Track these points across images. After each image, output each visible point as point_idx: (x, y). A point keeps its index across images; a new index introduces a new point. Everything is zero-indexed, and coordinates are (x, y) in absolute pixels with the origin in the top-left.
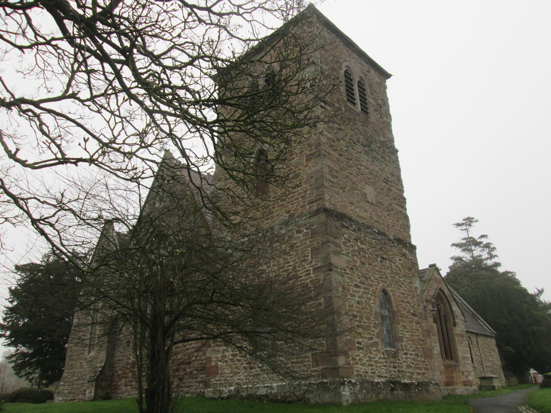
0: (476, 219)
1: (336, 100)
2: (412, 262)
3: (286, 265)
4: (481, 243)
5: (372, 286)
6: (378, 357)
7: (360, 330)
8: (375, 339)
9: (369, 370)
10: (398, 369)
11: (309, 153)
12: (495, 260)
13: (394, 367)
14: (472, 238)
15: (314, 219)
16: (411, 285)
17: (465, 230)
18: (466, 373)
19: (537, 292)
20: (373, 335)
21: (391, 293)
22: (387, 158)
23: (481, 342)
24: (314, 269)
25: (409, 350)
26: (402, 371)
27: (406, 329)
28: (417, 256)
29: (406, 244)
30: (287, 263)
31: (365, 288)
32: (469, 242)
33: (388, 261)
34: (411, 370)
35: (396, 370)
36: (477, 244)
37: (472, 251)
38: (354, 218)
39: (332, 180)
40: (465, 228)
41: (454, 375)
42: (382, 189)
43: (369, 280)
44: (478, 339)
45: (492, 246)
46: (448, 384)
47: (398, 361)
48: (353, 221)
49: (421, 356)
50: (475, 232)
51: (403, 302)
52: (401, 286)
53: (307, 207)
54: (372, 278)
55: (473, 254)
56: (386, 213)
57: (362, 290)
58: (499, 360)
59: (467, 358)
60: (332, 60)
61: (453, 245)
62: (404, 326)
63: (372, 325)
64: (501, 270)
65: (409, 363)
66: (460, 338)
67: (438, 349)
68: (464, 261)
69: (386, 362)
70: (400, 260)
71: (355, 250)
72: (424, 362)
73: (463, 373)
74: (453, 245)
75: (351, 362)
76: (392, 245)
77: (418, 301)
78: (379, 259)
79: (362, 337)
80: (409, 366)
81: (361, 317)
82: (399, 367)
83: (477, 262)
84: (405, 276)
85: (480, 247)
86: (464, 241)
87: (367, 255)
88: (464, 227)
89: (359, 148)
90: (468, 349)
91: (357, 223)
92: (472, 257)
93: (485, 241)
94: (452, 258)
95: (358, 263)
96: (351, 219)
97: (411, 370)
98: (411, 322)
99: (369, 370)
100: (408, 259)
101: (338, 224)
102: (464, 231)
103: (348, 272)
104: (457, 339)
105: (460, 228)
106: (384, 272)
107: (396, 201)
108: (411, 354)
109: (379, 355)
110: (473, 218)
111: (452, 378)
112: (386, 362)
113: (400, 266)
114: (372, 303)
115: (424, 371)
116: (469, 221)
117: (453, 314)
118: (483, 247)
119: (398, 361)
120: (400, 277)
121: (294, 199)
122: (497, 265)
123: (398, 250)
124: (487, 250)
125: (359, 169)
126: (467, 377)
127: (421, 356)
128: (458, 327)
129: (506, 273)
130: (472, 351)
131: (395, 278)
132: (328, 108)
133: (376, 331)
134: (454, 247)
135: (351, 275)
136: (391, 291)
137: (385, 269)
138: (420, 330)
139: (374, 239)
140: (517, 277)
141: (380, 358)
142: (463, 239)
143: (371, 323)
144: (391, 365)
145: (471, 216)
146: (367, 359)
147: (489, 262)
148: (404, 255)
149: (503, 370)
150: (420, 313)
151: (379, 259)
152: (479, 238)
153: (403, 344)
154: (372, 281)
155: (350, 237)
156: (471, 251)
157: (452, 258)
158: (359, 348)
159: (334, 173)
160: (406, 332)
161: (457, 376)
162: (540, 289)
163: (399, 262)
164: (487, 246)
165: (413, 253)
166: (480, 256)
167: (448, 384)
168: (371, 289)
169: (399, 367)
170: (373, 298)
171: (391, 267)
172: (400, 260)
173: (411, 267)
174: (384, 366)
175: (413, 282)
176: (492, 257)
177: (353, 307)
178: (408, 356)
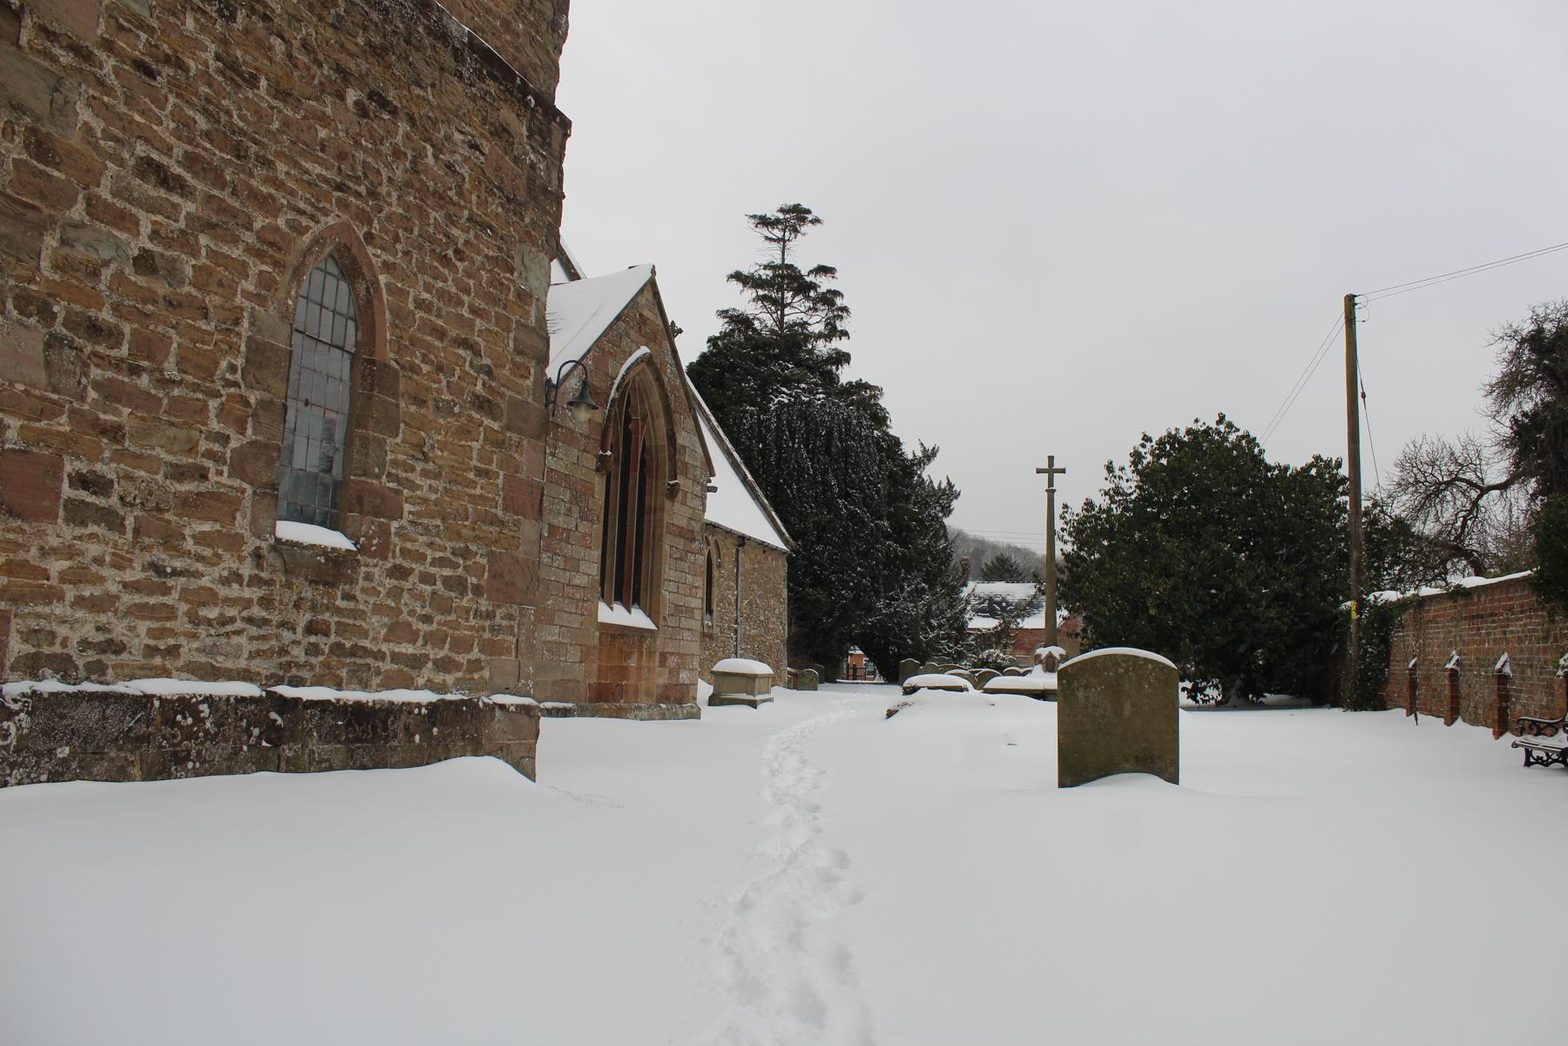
0: (815, 214)
2: (531, 181)
4: (813, 286)
5: (266, 204)
6: (220, 571)
8: (221, 479)
10: (333, 638)
12: (838, 344)
13: (311, 629)
14: (790, 267)
16: (504, 276)
17: (778, 240)
18: (672, 661)
19: (919, 454)
20: (210, 454)
21: (383, 279)
23: (748, 566)
25: (421, 558)
27: (426, 458)
28: (567, 165)
29: (524, 90)
32: (783, 277)
33: (403, 127)
35: (324, 643)
36: (803, 288)
37: (784, 306)
40: (780, 235)
43: (259, 171)
44: (741, 556)
45: (839, 302)
47: (340, 603)
49: (477, 590)
50: (803, 254)
51: (441, 334)
52: (445, 260)
54: (282, 168)
55: (783, 315)
57: (189, 207)
58: (785, 622)
59: (690, 610)
61: (738, 276)
62: (420, 446)
63: (213, 404)
64: (846, 375)
65: (404, 617)
66: (680, 543)
67: (595, 570)
68: (755, 330)
69: (266, 602)
70: (475, 147)
71: (526, 327)
72: (490, 615)
74: (738, 276)
76: (450, 62)
77: (519, 352)
78: (352, 96)
79: (120, 456)
80: (398, 631)
81: (150, 347)
82: (342, 629)
83: (792, 341)
84: (484, 226)
85: (808, 298)
86: (767, 274)
88: (777, 233)
90: (700, 582)
92: (780, 322)
93: (825, 284)
94: (723, 313)
97: (408, 649)
98: (465, 432)
100: (516, 160)
102: (774, 245)
104: (669, 543)
105: (765, 231)
108: (427, 578)
110: (809, 212)
111: (623, 672)
112: (266, 602)
113: (465, 171)
114: (246, 295)
115: (475, 654)
116: (796, 217)
117: (672, 456)
118: (815, 301)
119: (340, 603)
120: (451, 220)
122: (842, 358)
123: (473, 98)
124: (823, 313)
126: (674, 672)
127: (477, 590)
128: (684, 503)
129: (861, 386)
130: (715, 590)
131: (423, 215)
133: (234, 444)
134: (734, 282)
135: (129, 100)
137: (377, 154)
138: (500, 481)
140: (882, 402)
141: (236, 577)
142: (765, 267)
143: (216, 394)
144: (292, 615)
145: (805, 206)
146: (135, 574)
147: (822, 348)
148: (501, 132)
149: (789, 650)
150: (516, 406)
151: (352, 96)
152: (811, 272)
153: (395, 525)
154: (279, 185)
156: (781, 305)
157: (723, 313)
158: (78, 514)
160: (425, 474)
161: (639, 668)
162: (929, 447)
163: (466, 151)
164: (829, 299)
165: (546, 143)
166: (804, 325)
169: (342, 629)
170: (257, 267)
171: (419, 155)
172: (475, 147)
173: (522, 196)
174: (250, 620)
175: (517, 263)
176: (832, 332)
177: (95, 274)
178: (408, 585)
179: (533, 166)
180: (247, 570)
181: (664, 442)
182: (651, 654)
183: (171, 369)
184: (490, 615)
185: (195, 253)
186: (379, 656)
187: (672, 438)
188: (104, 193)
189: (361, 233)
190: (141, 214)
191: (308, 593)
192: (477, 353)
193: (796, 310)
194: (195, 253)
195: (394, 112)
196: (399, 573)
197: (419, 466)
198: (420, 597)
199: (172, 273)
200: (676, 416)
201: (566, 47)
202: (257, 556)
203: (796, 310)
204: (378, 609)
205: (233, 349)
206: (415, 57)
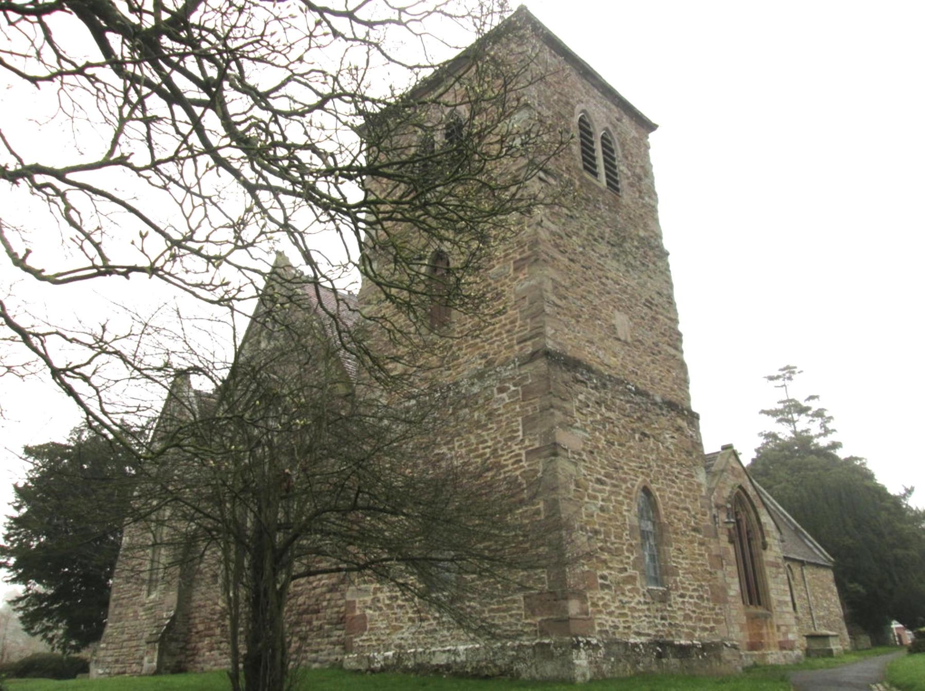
1: (564, 168)
3: (481, 446)
4: (808, 409)
5: (624, 481)
6: (636, 600)
7: (606, 556)
9: (620, 623)
10: (669, 621)
11: (518, 257)
14: (792, 400)
15: (527, 369)
18: (783, 629)
20: (627, 563)
21: (657, 494)
22: (651, 265)
24: (528, 453)
25: (688, 589)
26: (676, 625)
29: (683, 410)
30: (482, 442)
31: (614, 486)
34: (690, 623)
36: (802, 410)
38: (595, 366)
39: (558, 302)
40: (783, 383)
41: (764, 631)
42: (643, 318)
43: (621, 471)
45: (827, 414)
46: (753, 646)
47: (669, 608)
48: (593, 372)
49: (708, 599)
50: (798, 391)
51: (677, 508)
52: (673, 482)
53: (517, 348)
54: (625, 467)
56: (648, 359)
57: (608, 488)
58: (840, 606)
59: (786, 603)
60: (559, 100)
62: (679, 550)
65: (687, 612)
66: (774, 570)
69: (649, 609)
70: (673, 437)
72: (713, 609)
73: (778, 627)
75: (590, 609)
76: (659, 411)
80: (687, 617)
81: (607, 534)
82: (671, 618)
83: (803, 441)
84: (681, 465)
85: (807, 415)
86: (781, 406)
87: (617, 430)
89: (604, 248)
91: (600, 376)
92: (795, 432)
93: (815, 405)
94: (761, 434)
95: (602, 443)
96: (589, 369)
97: (690, 623)
99: (620, 623)
100: (686, 436)
101: (567, 376)
103: (584, 457)
104: (768, 571)
106: (646, 458)
107: (666, 339)
108: (691, 597)
109: (637, 598)
110: (795, 367)
111: (761, 636)
112: (649, 609)
113: (672, 447)
115: (712, 624)
116: (789, 371)
118: (813, 416)
120: (672, 466)
121: (494, 333)
124: (819, 421)
125: (603, 284)
126: (785, 634)
127: (708, 599)
128: (771, 550)
129: (851, 459)
130: (795, 592)
131: (663, 467)
132: (552, 181)
133: (632, 558)
134: (764, 415)
136: (658, 489)
137: (648, 452)
139: (628, 402)
141: (639, 602)
143: (624, 544)
145: (791, 365)
146: (617, 604)
147: (823, 442)
148: (679, 429)
149: (847, 624)
150: (707, 527)
153: (678, 579)
154: (626, 473)
155: (587, 398)
157: (761, 434)
158: (603, 587)
159: (562, 291)
160: (683, 558)
161: (768, 634)
164: (819, 414)
165: (694, 426)
167: (753, 646)
168: (624, 486)
169: (671, 618)
170: (626, 501)
171: (658, 449)
173: (691, 449)
174: (646, 616)
175: (694, 474)
176: (827, 432)
179: (692, 436)
180: (642, 600)
181: (755, 523)
182: (772, 627)
183: (613, 538)
184: (713, 609)
185: (611, 502)
186: (682, 626)
187: (758, 519)
188: (590, 491)
189: (648, 480)
190: (598, 494)
191: (659, 606)
192: (689, 512)
193: (803, 423)
194: (611, 502)
195: (649, 437)
196: (682, 596)
197: (681, 556)
198: (690, 603)
199: (608, 511)
200: (758, 510)
201: (690, 386)
202: (644, 595)
203: (803, 423)
204: (679, 609)
205: (626, 529)
206: (650, 414)
